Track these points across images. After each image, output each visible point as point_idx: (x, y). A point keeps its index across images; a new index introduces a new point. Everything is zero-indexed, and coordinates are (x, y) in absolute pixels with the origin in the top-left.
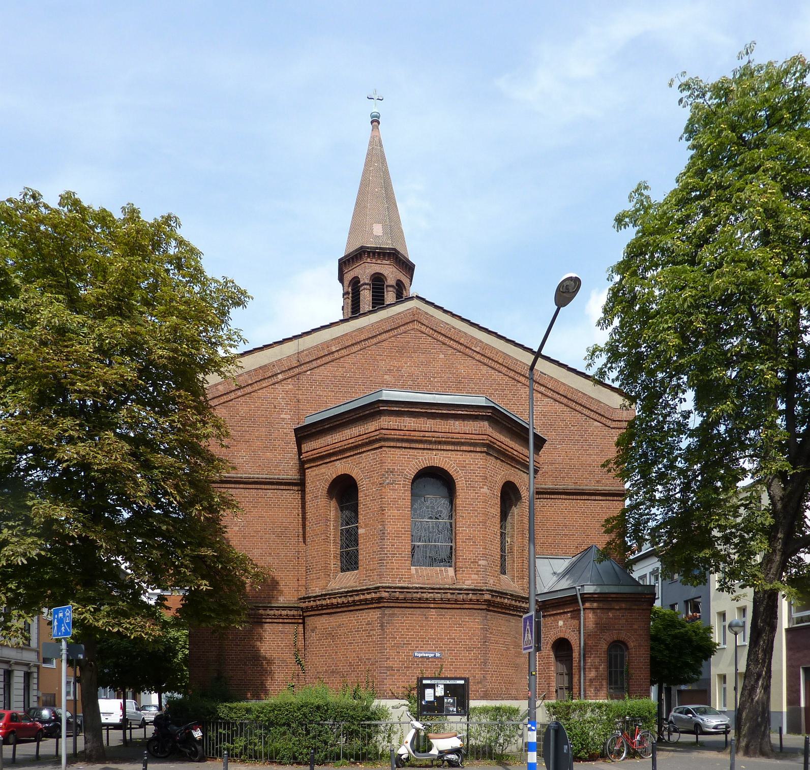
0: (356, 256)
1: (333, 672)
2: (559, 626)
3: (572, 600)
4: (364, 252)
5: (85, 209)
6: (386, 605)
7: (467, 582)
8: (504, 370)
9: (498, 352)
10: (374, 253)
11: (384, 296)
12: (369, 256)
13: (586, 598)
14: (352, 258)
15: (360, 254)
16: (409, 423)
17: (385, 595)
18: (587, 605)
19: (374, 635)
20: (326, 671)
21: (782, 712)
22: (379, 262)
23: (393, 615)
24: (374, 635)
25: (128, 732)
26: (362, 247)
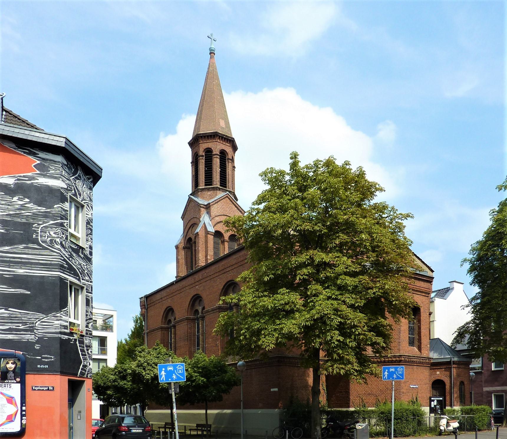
0: (211, 136)
1: (369, 394)
2: (439, 374)
3: (449, 363)
4: (217, 135)
5: (496, 221)
7: (425, 354)
10: (222, 138)
11: (226, 164)
12: (219, 139)
13: (454, 363)
14: (208, 136)
15: (214, 136)
17: (403, 359)
18: (454, 366)
20: (365, 394)
21: (349, 407)
22: (224, 143)
26: (216, 132)
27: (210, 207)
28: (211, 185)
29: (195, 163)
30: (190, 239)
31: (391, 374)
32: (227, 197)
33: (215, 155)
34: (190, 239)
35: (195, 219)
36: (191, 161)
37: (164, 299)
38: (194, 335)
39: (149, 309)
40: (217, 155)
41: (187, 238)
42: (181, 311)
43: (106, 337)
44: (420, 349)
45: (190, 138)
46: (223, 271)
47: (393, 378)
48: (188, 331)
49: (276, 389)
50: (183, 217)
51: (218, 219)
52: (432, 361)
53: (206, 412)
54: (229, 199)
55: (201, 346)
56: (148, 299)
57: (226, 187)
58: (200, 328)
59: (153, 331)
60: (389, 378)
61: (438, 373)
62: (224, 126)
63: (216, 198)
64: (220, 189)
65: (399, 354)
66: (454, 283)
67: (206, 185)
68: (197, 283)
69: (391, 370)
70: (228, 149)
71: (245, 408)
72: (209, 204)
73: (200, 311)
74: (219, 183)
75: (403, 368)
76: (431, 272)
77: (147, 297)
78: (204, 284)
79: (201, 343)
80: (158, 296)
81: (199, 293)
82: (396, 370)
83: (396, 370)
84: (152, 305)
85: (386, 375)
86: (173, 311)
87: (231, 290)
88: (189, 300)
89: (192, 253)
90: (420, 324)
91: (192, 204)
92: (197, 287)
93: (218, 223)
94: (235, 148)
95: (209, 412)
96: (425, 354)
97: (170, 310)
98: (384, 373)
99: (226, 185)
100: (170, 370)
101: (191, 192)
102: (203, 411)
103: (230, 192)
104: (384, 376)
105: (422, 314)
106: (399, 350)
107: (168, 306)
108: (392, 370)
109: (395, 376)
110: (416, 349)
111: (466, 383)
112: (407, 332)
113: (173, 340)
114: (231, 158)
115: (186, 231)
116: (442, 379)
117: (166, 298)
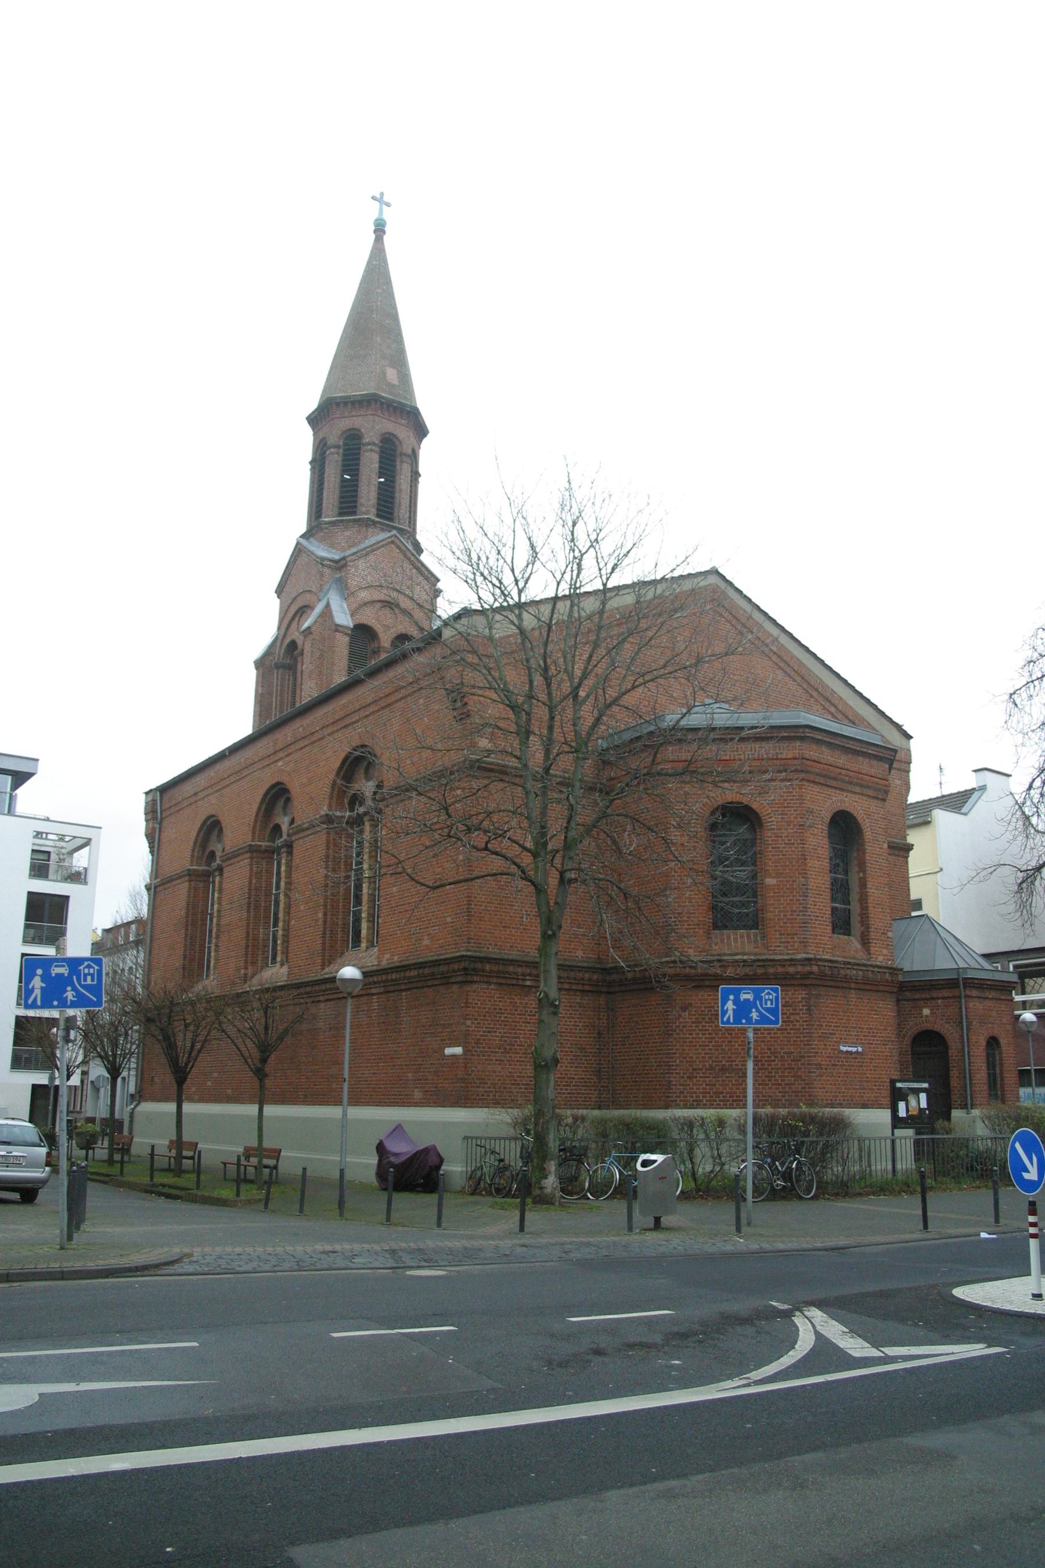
1: (723, 1069)
6: (814, 982)
7: (880, 958)
8: (798, 679)
9: (793, 657)
11: (395, 466)
14: (353, 403)
15: (369, 402)
16: (827, 755)
17: (815, 969)
19: (797, 1021)
20: (711, 1068)
23: (818, 996)
24: (797, 1021)
25: (91, 1152)
27: (345, 565)
28: (354, 513)
29: (318, 464)
30: (293, 645)
31: (743, 1009)
32: (393, 542)
33: (369, 444)
34: (293, 645)
35: (308, 595)
36: (309, 456)
37: (201, 795)
38: (268, 893)
39: (165, 823)
40: (374, 444)
41: (287, 641)
42: (238, 831)
43: (67, 898)
44: (865, 942)
45: (312, 404)
46: (342, 723)
47: (749, 1020)
48: (250, 883)
49: (458, 1050)
50: (280, 591)
51: (364, 595)
52: (900, 978)
53: (261, 1110)
54: (398, 547)
55: (281, 924)
56: (166, 797)
57: (391, 520)
58: (283, 875)
59: (171, 880)
60: (737, 1019)
61: (926, 1012)
62: (396, 382)
63: (363, 546)
64: (374, 523)
65: (804, 956)
66: (986, 772)
67: (341, 514)
68: (281, 755)
69: (744, 997)
70: (403, 433)
71: (356, 1100)
72: (344, 558)
73: (285, 828)
74: (374, 511)
75: (776, 991)
76: (903, 739)
77: (164, 789)
78: (295, 756)
79: (281, 915)
80: (188, 788)
81: (285, 779)
82: (758, 997)
83: (758, 997)
84: (173, 810)
85: (730, 1013)
86: (221, 830)
87: (362, 771)
88: (258, 799)
89: (295, 679)
90: (864, 872)
91: (304, 559)
92: (280, 763)
93: (365, 604)
94: (421, 431)
95: (270, 1110)
96: (880, 958)
97: (212, 827)
98: (724, 1003)
99: (392, 514)
100: (60, 976)
101: (303, 529)
102: (253, 1109)
103: (401, 531)
104: (724, 1012)
105: (868, 848)
106: (804, 944)
107: (213, 812)
108: (747, 996)
109: (754, 1015)
110: (855, 944)
111: (1003, 1042)
112: (827, 895)
113: (216, 906)
114: (410, 452)
115: (285, 625)
116: (937, 1028)
117: (205, 793)
